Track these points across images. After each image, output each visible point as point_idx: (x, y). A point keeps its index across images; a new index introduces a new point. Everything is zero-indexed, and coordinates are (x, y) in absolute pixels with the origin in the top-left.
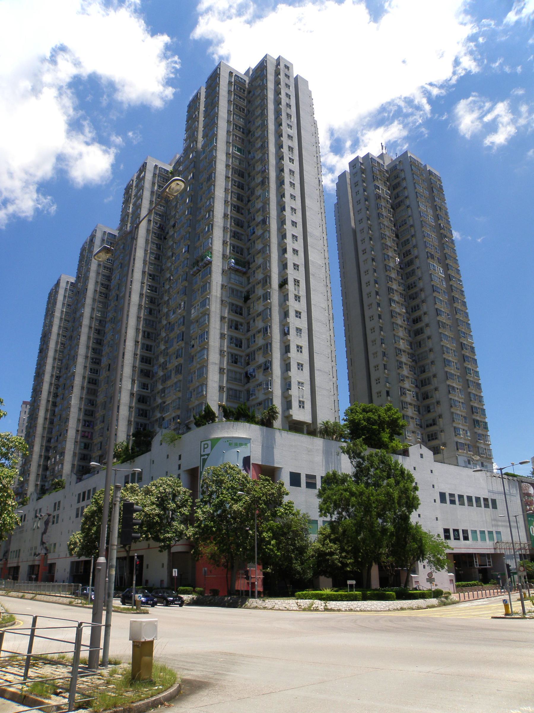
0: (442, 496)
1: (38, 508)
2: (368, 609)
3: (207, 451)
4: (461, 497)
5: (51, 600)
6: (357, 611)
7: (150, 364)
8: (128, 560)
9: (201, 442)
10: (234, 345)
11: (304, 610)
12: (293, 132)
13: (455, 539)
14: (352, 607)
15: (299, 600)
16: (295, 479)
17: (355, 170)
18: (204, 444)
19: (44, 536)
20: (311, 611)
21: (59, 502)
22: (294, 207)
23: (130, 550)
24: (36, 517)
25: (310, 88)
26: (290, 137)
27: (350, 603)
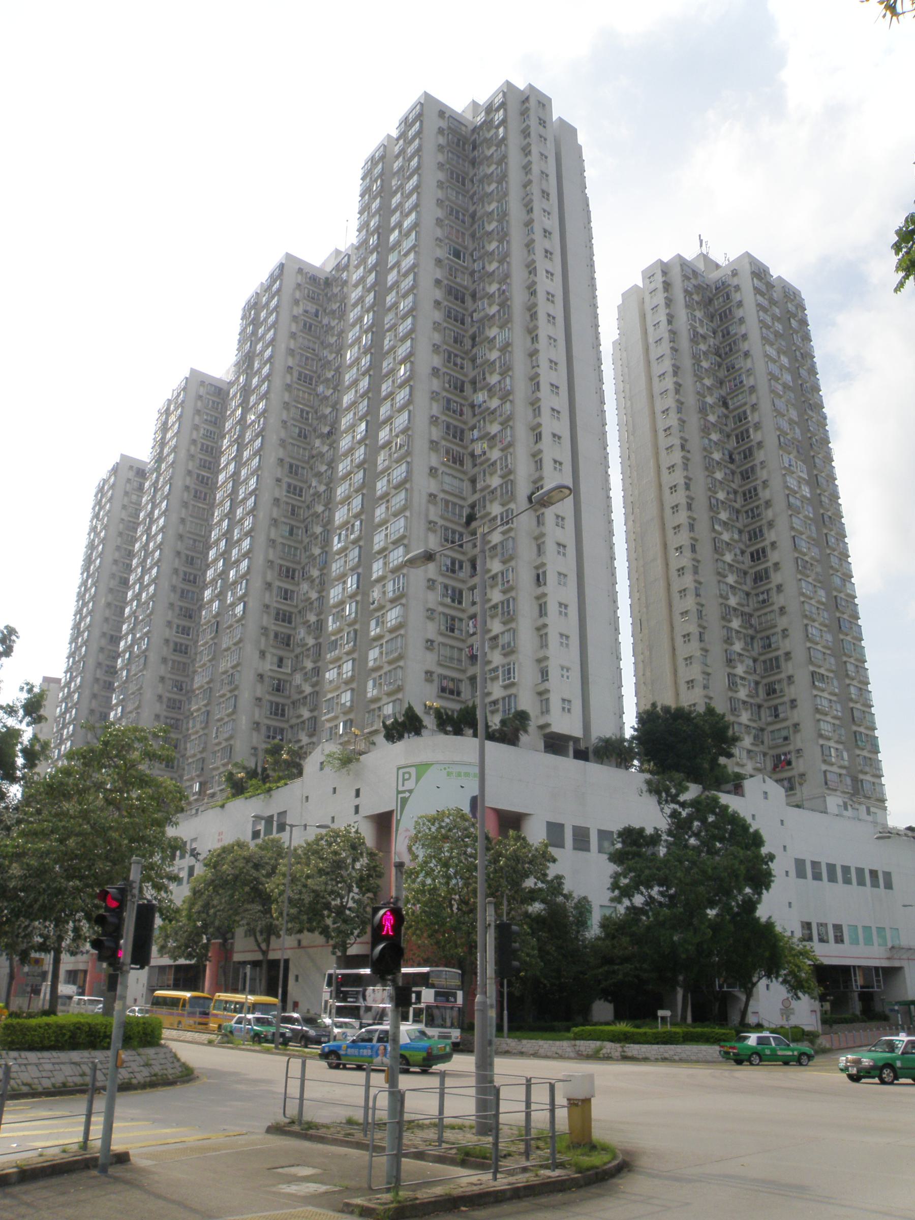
2: (693, 1058)
3: (409, 785)
4: (831, 868)
5: (198, 1040)
7: (290, 622)
8: (265, 966)
9: (398, 769)
10: (449, 600)
12: (552, 224)
14: (667, 1055)
15: (578, 1042)
17: (653, 286)
18: (404, 774)
20: (600, 1059)
22: (554, 359)
26: (547, 233)
27: (662, 1048)
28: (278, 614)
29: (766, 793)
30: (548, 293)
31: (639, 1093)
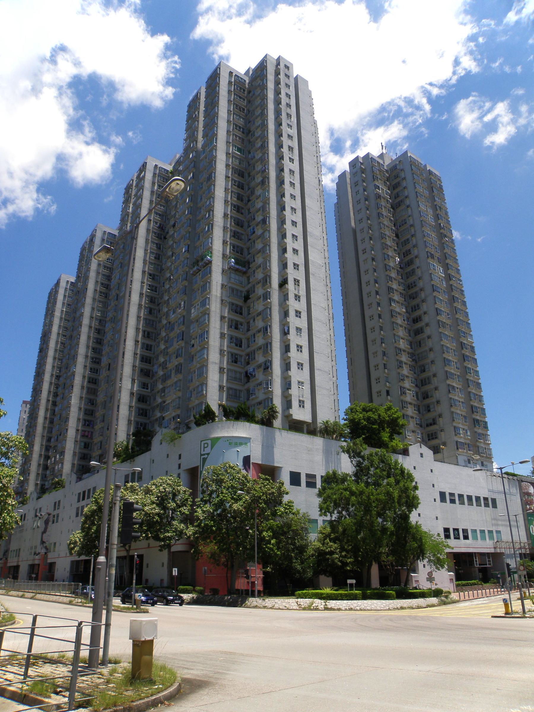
0: (442, 495)
1: (38, 507)
2: (368, 608)
3: (207, 450)
4: (461, 496)
5: (51, 599)
6: (357, 610)
7: (150, 363)
8: (128, 559)
9: (201, 441)
10: (234, 345)
11: (304, 609)
12: (293, 132)
13: (455, 538)
14: (352, 607)
15: (299, 599)
16: (295, 479)
17: (355, 170)
18: (204, 444)
19: (44, 535)
20: (311, 610)
21: (59, 502)
22: (294, 206)
23: (130, 549)
24: (36, 516)
25: (310, 88)
26: (290, 137)
27: (350, 602)
31: (183, 631)
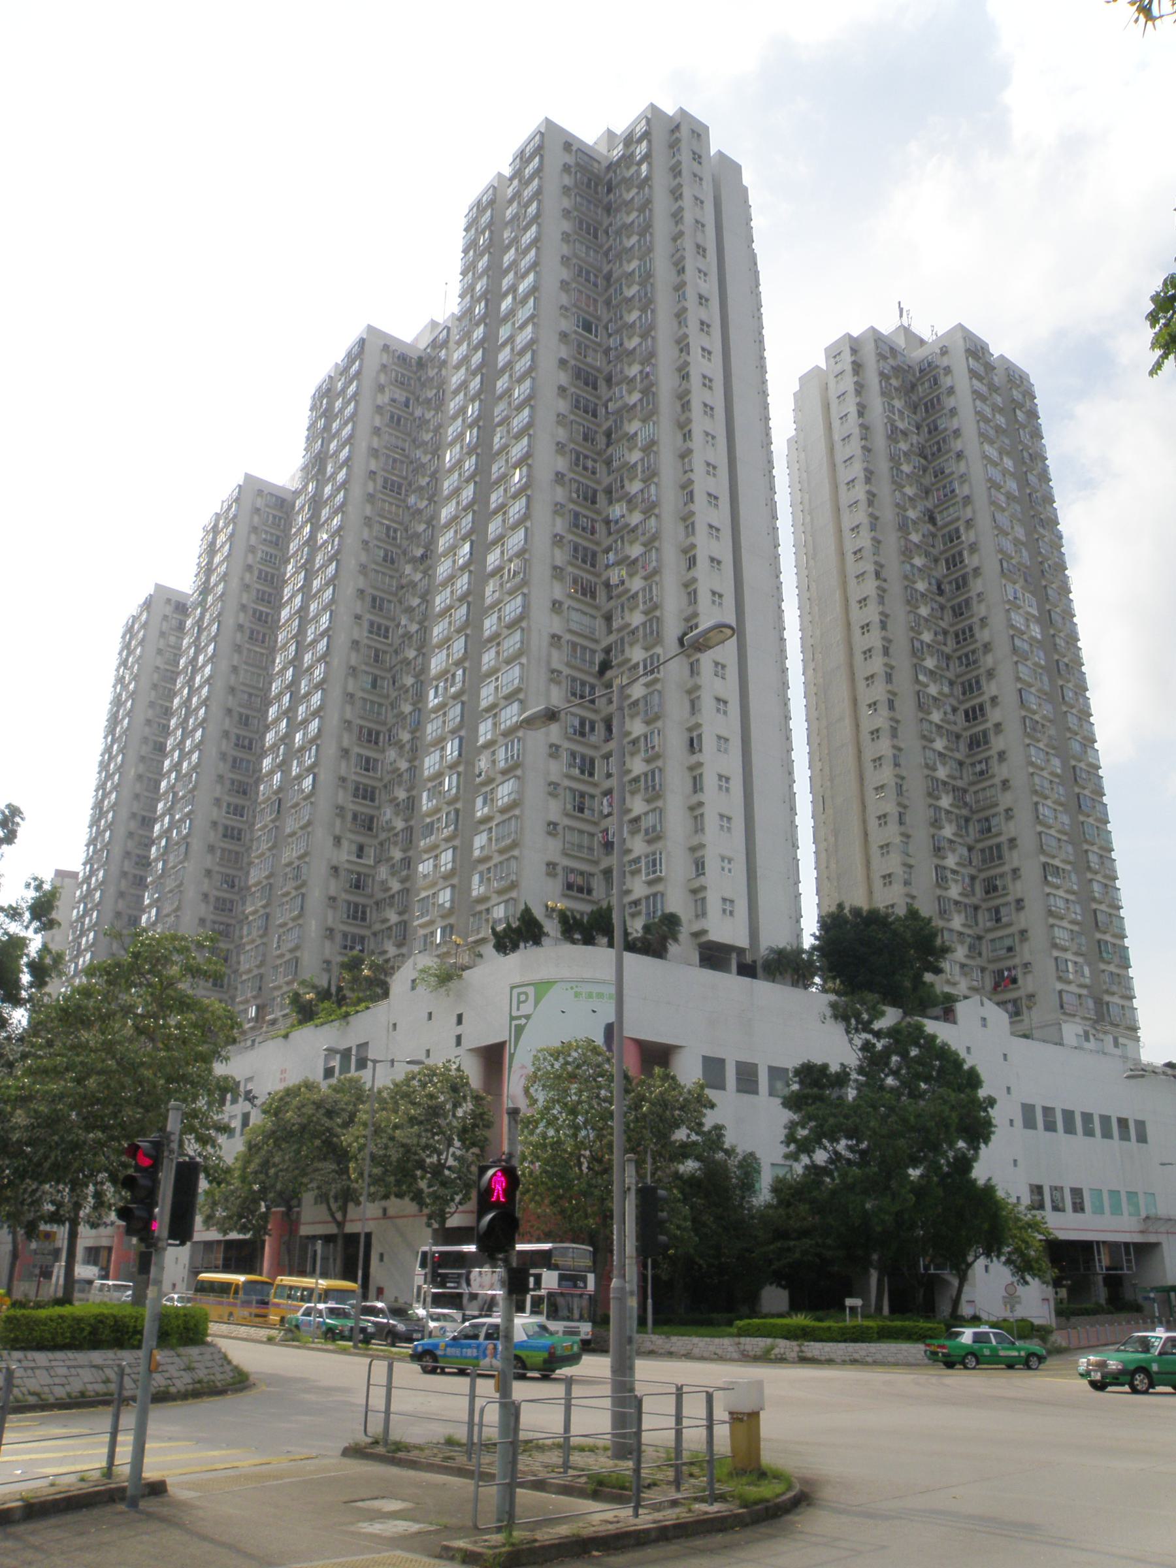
2: (891, 1359)
3: (526, 1009)
4: (1068, 1115)
5: (254, 1336)
7: (372, 800)
8: (340, 1242)
9: (512, 988)
10: (577, 771)
12: (710, 287)
14: (857, 1356)
15: (742, 1340)
17: (839, 368)
18: (519, 994)
20: (771, 1361)
22: (712, 461)
26: (702, 299)
27: (851, 1347)
28: (357, 789)
29: (984, 1019)
30: (704, 377)
